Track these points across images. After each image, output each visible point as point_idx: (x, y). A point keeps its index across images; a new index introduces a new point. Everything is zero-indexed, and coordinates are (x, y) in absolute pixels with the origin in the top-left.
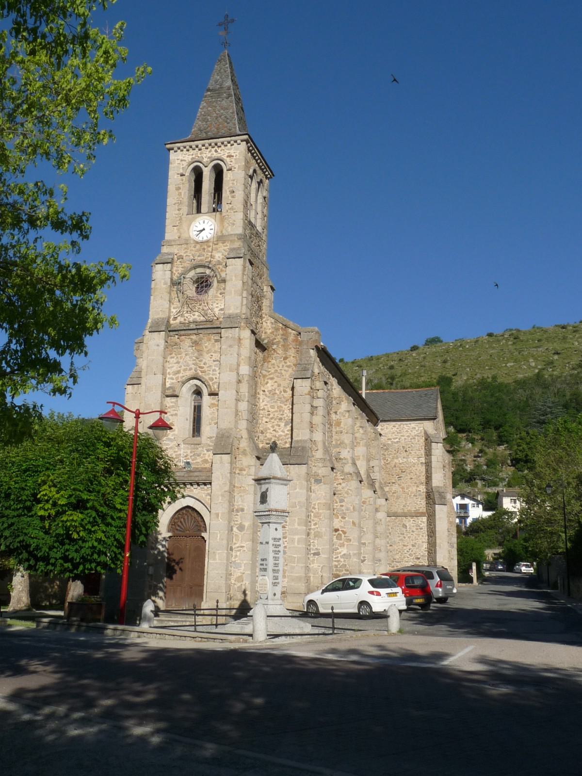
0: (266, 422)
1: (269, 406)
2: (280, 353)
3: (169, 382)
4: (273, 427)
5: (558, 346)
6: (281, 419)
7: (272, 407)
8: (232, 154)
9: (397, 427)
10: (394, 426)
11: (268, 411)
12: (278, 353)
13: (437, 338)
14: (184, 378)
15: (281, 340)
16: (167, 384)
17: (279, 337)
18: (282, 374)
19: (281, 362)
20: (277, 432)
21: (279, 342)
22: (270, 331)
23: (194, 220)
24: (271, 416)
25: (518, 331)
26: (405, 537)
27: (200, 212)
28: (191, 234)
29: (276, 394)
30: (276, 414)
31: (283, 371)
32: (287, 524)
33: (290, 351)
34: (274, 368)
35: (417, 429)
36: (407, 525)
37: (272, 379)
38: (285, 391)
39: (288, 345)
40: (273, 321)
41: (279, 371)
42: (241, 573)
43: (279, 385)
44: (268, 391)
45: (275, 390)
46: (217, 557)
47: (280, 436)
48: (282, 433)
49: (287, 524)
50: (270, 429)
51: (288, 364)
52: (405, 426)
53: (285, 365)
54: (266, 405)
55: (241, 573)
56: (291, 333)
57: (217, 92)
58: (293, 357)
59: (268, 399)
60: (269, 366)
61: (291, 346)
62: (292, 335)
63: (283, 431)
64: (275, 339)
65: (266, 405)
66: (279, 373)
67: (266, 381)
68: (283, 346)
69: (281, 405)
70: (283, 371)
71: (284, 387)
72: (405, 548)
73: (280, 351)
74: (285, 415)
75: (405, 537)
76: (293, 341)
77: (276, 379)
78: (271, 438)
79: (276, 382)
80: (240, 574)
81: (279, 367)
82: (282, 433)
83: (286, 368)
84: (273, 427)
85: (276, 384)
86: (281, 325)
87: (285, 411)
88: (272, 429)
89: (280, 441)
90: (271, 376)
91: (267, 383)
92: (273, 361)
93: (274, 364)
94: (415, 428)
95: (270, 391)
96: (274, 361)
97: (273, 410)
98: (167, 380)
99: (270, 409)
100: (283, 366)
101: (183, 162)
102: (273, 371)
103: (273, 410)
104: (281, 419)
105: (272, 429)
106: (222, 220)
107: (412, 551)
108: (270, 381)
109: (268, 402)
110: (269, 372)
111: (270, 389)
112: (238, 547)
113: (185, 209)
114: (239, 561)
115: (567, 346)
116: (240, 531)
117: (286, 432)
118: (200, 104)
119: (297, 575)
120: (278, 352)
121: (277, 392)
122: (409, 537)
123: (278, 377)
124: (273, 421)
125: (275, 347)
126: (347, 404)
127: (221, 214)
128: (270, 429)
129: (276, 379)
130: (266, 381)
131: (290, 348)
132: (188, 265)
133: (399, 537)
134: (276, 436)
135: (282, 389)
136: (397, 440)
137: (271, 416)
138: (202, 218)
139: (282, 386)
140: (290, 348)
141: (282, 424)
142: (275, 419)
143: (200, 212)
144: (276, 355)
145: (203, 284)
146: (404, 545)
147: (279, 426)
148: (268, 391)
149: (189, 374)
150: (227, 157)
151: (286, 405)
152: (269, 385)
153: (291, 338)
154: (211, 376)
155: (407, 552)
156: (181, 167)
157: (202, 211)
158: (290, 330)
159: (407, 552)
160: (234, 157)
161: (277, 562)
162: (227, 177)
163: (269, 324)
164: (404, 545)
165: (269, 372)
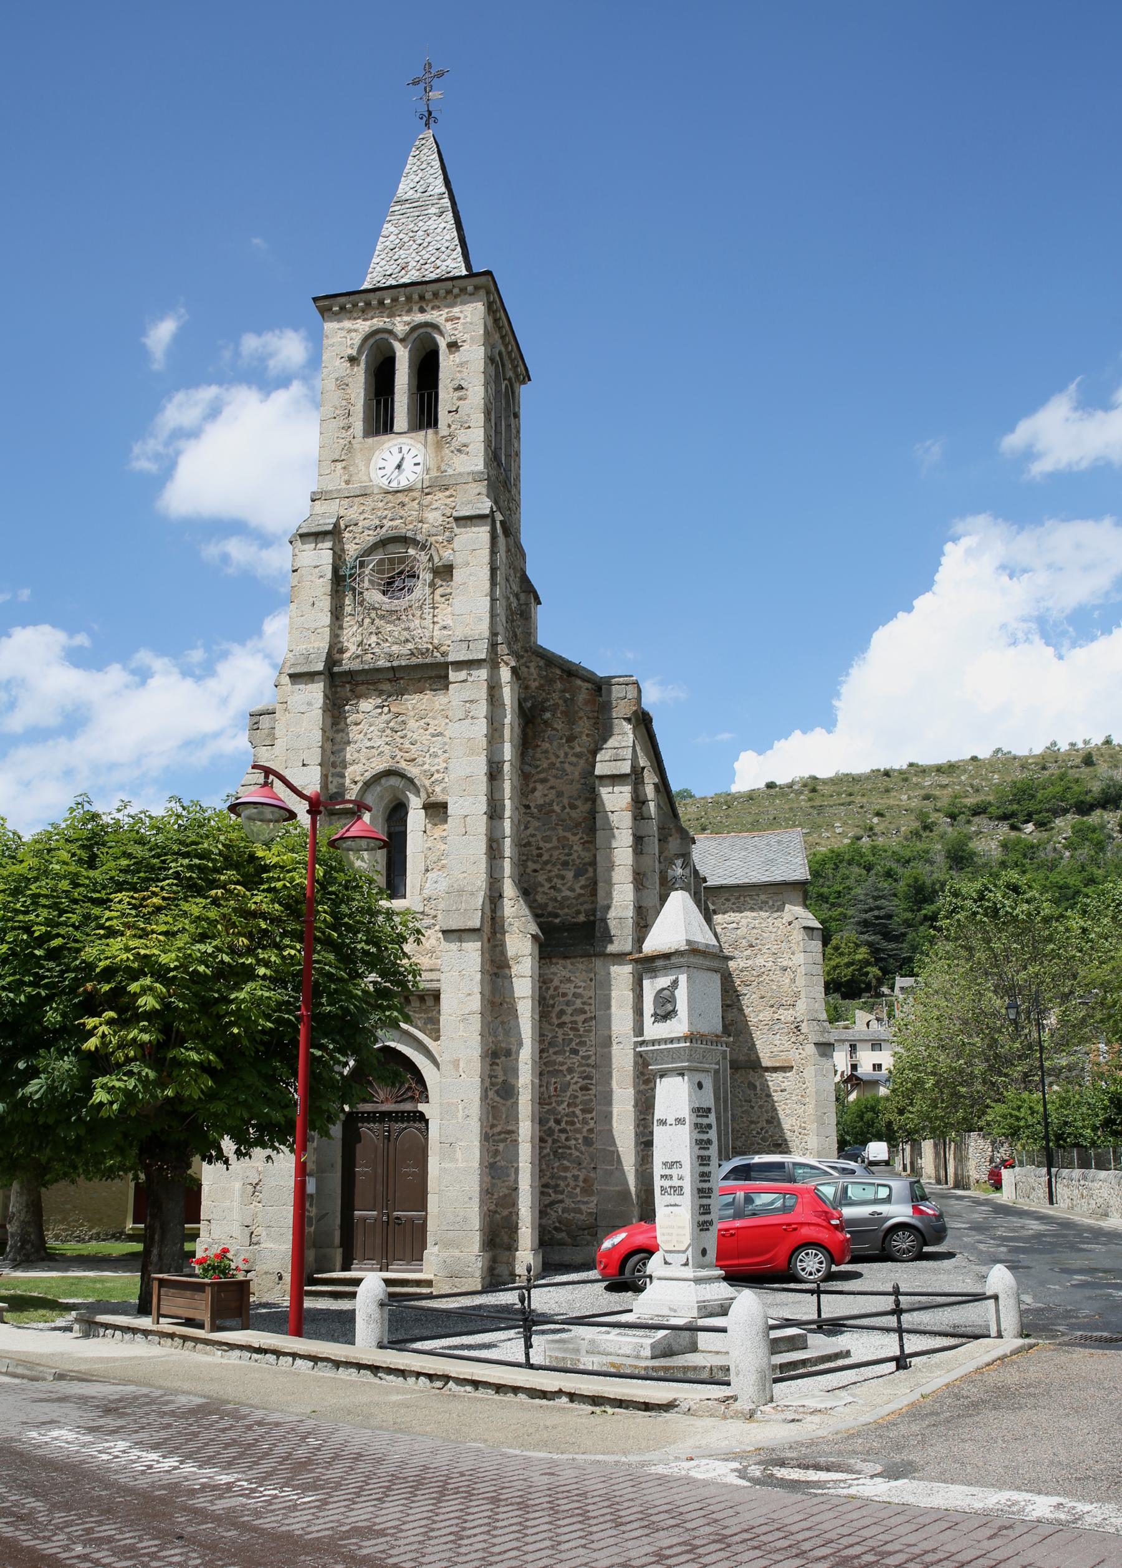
0: (535, 871)
1: (539, 837)
2: (559, 727)
3: (335, 783)
4: (549, 880)
5: (879, 803)
6: (565, 864)
7: (547, 839)
8: (457, 315)
9: (733, 901)
10: (728, 900)
11: (539, 848)
12: (555, 729)
13: (686, 791)
14: (366, 774)
15: (561, 702)
16: (330, 786)
17: (556, 696)
18: (564, 770)
19: (560, 746)
20: (559, 890)
21: (556, 705)
22: (537, 684)
23: (372, 450)
24: (545, 857)
25: (815, 778)
26: (752, 1107)
27: (391, 431)
28: (373, 476)
29: (553, 811)
30: (556, 853)
31: (566, 766)
32: (594, 1082)
33: (581, 723)
34: (548, 759)
35: (771, 903)
36: (758, 1084)
37: (544, 781)
38: (573, 807)
39: (577, 712)
40: (542, 663)
41: (558, 765)
42: (508, 1188)
43: (560, 794)
44: (537, 806)
45: (551, 804)
46: (459, 1155)
47: (566, 898)
48: (568, 893)
49: (594, 1082)
50: (543, 886)
51: (578, 749)
52: (748, 899)
53: (571, 752)
54: (533, 836)
55: (508, 1188)
56: (580, 688)
57: (419, 206)
58: (587, 735)
59: (537, 824)
60: (538, 756)
61: (581, 714)
62: (584, 691)
63: (572, 889)
64: (548, 700)
65: (533, 836)
66: (557, 769)
67: (531, 786)
68: (565, 713)
69: (566, 834)
70: (566, 766)
71: (570, 797)
72: (753, 1126)
73: (559, 725)
74: (575, 856)
75: (752, 1107)
76: (587, 703)
77: (553, 781)
78: (547, 905)
79: (552, 788)
80: (507, 1192)
81: (558, 757)
82: (568, 893)
83: (574, 759)
84: (549, 880)
85: (554, 792)
86: (558, 672)
87: (575, 848)
88: (547, 885)
89: (566, 910)
90: (542, 776)
91: (534, 790)
92: (546, 745)
93: (546, 752)
94: (767, 902)
95: (540, 807)
96: (547, 745)
97: (549, 846)
98: (330, 779)
99: (542, 844)
100: (566, 754)
101: (353, 334)
102: (545, 766)
103: (549, 846)
104: (565, 864)
105: (547, 885)
106: (439, 445)
107: (767, 1132)
108: (539, 786)
109: (536, 829)
110: (537, 767)
111: (540, 802)
112: (500, 1133)
113: (358, 426)
114: (503, 1163)
115: (892, 802)
116: (502, 1097)
117: (578, 891)
118: (378, 234)
119: (617, 1188)
120: (555, 726)
121: (557, 808)
122: (761, 1107)
123: (556, 777)
124: (549, 867)
125: (548, 715)
126: (679, 841)
127: (437, 433)
128: (543, 886)
129: (553, 781)
130: (531, 786)
131: (581, 718)
132: (370, 538)
133: (741, 1106)
134: (556, 900)
135: (566, 801)
136: (734, 925)
137: (545, 857)
138: (395, 442)
139: (566, 795)
140: (581, 718)
141: (570, 875)
142: (554, 865)
143: (391, 431)
144: (549, 732)
145: (396, 579)
146: (752, 1122)
147: (563, 878)
148: (537, 806)
149: (380, 765)
150: (447, 320)
151: (575, 834)
152: (537, 794)
153: (582, 697)
154: (426, 767)
155: (758, 1133)
156: (349, 343)
157: (396, 428)
158: (579, 682)
159: (758, 1133)
160: (461, 321)
161: (705, 1201)
162: (447, 362)
163: (532, 670)
164: (752, 1122)
165: (537, 767)
